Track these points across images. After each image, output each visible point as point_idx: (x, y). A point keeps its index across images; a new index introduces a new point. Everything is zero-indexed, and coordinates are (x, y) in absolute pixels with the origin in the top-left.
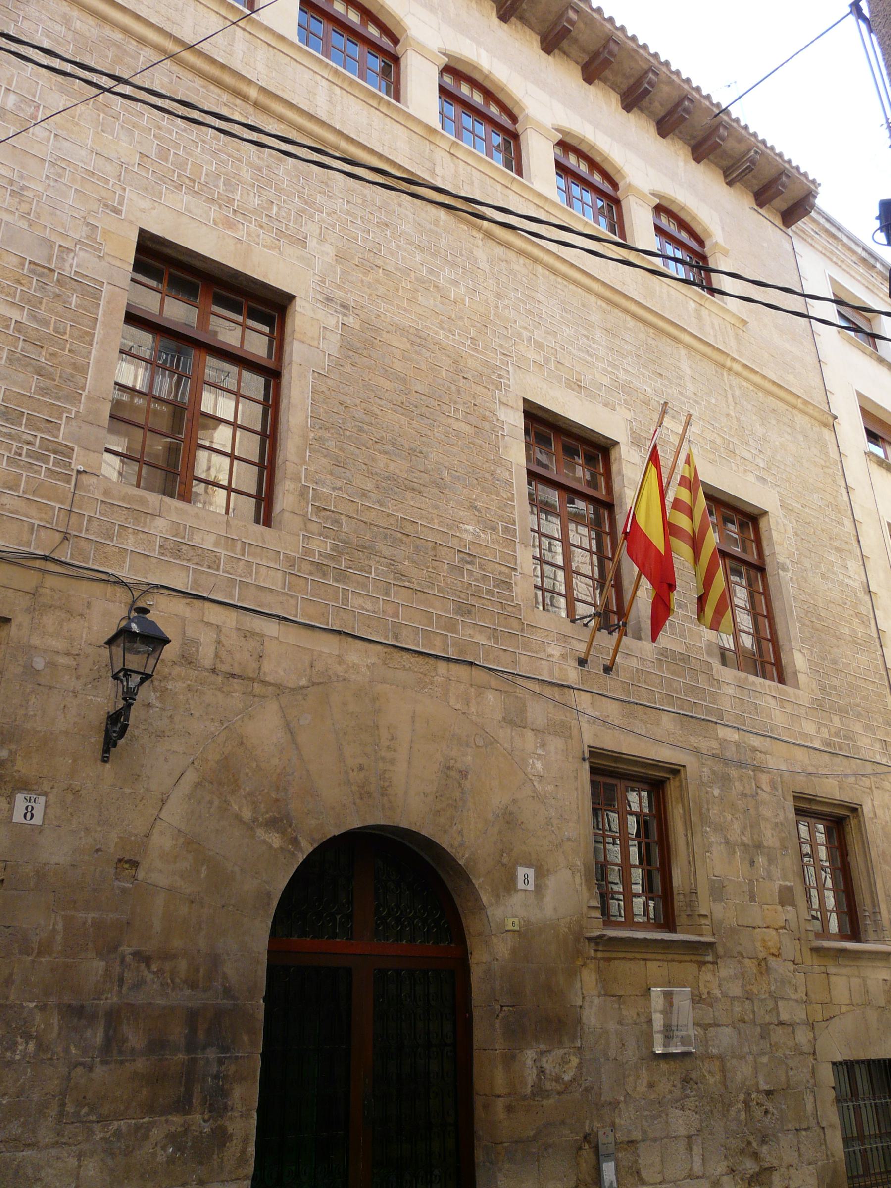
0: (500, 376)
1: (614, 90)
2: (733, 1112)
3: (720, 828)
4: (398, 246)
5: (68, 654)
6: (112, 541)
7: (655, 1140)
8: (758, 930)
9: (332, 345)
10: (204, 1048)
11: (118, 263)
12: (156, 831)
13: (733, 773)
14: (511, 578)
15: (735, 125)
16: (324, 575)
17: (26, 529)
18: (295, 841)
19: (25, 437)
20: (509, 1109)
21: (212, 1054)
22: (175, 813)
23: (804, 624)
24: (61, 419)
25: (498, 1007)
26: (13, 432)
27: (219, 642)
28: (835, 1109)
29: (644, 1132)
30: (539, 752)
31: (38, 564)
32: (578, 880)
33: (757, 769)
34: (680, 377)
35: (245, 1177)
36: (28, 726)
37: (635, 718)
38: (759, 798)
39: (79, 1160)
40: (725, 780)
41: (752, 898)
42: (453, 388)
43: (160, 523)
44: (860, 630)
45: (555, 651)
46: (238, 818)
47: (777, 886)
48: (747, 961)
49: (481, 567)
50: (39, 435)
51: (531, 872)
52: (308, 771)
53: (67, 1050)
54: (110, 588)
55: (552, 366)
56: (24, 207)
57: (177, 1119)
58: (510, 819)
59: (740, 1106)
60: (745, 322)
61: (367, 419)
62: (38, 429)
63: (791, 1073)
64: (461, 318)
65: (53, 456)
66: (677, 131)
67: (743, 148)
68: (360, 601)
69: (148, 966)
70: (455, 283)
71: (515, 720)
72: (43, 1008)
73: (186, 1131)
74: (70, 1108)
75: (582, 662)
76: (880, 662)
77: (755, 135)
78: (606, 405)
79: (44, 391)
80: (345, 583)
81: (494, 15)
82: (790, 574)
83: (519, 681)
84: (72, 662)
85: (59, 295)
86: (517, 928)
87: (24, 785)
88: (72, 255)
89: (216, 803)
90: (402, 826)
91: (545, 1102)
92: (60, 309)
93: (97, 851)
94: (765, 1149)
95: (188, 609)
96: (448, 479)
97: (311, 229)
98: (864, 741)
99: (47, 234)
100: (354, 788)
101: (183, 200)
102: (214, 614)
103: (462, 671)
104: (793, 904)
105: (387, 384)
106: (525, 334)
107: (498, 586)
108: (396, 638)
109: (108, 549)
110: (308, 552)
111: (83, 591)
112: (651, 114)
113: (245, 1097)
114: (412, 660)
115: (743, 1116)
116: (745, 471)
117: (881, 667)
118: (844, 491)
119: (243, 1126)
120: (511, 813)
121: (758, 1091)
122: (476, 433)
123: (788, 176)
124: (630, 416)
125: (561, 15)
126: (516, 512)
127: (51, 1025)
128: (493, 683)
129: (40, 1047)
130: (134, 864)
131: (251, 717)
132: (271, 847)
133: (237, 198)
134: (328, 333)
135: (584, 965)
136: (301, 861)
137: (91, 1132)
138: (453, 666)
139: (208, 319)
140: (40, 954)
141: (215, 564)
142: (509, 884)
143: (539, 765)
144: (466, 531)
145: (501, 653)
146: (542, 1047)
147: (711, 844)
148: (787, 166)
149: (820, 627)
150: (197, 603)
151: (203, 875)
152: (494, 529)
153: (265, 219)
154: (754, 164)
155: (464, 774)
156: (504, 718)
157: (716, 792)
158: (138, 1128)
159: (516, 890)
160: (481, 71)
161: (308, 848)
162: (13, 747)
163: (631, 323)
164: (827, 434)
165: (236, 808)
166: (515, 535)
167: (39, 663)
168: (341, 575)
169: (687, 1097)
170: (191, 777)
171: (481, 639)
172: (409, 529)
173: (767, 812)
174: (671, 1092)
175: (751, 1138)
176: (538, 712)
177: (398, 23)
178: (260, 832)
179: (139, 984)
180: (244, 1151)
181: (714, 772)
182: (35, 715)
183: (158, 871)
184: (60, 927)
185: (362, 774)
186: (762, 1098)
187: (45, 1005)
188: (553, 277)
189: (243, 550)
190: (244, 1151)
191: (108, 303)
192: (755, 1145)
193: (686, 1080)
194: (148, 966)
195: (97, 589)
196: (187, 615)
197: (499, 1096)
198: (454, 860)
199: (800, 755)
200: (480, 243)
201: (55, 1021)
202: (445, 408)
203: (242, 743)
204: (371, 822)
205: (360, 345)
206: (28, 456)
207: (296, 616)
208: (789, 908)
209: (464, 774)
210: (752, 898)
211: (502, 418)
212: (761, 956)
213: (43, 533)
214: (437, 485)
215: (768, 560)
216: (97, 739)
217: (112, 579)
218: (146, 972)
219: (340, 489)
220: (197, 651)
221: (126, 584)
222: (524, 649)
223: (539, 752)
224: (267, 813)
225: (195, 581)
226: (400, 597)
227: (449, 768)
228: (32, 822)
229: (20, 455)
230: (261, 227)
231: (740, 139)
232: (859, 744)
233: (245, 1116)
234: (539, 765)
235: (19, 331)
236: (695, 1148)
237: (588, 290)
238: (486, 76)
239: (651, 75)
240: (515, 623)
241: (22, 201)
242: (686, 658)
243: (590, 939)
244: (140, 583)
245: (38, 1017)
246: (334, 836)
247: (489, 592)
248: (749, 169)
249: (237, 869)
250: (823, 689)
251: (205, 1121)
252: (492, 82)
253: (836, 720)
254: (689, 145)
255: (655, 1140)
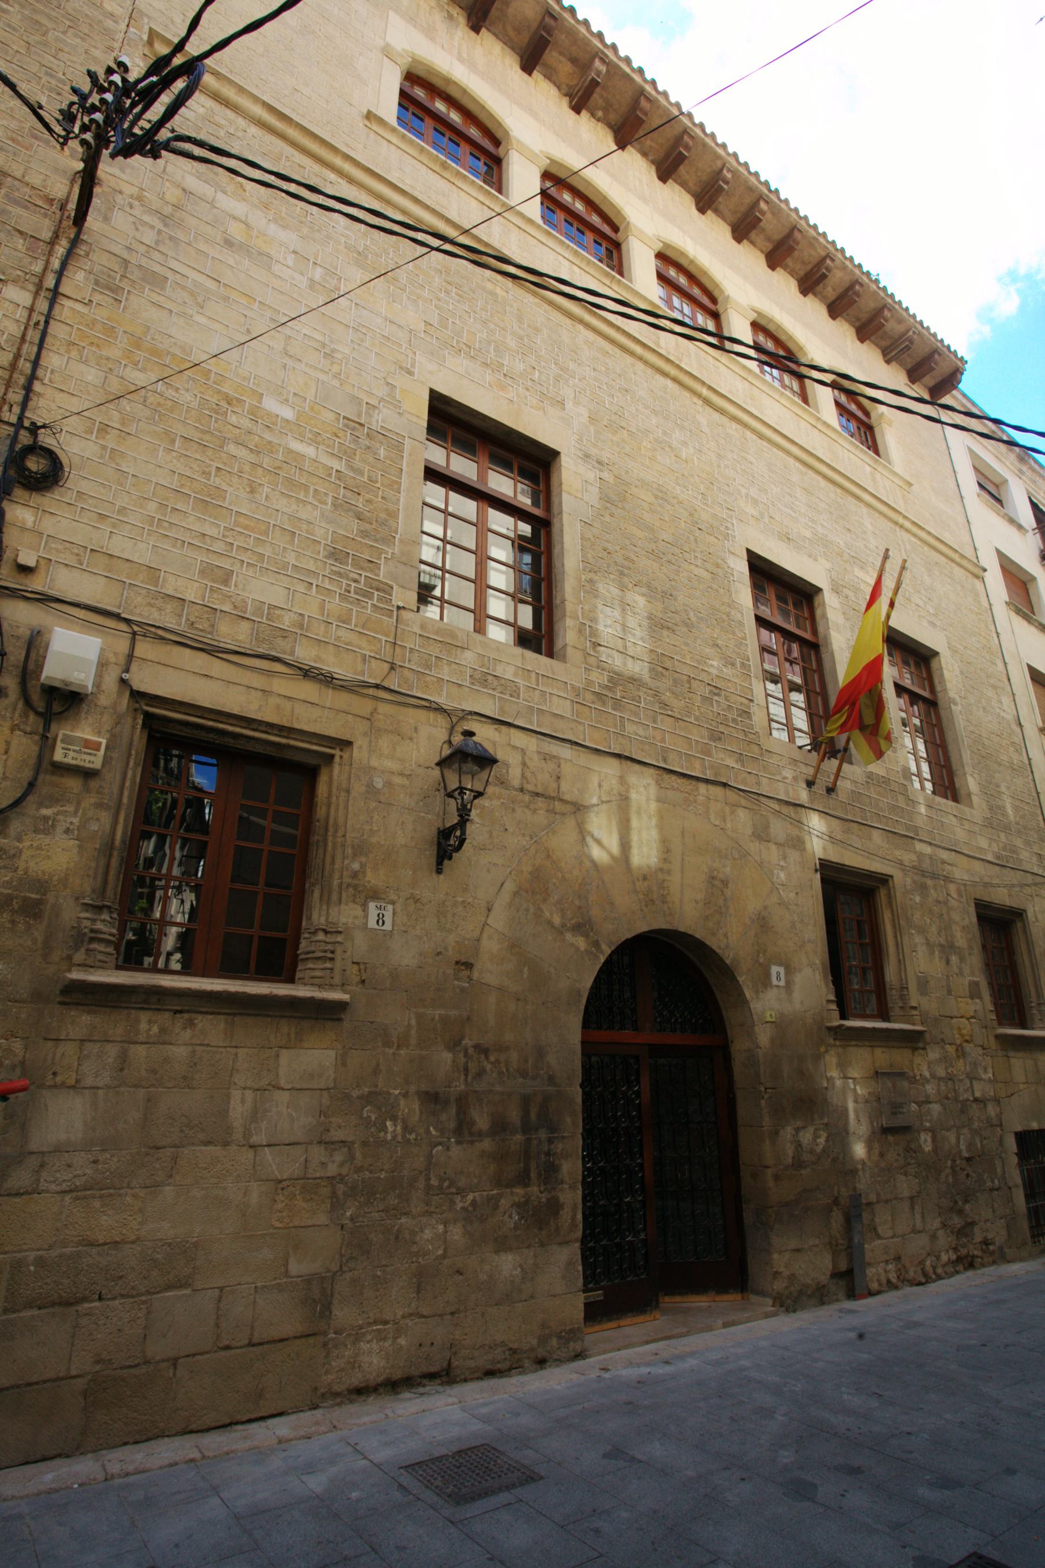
0: (727, 528)
1: (793, 276)
2: (943, 1175)
3: (922, 931)
4: (637, 410)
5: (401, 774)
6: (431, 670)
7: (887, 1201)
8: (954, 1020)
9: (592, 496)
10: (537, 1130)
11: (415, 419)
12: (485, 935)
13: (930, 882)
14: (749, 708)
15: (897, 307)
16: (604, 704)
17: (359, 659)
18: (596, 944)
19: (352, 575)
20: (777, 1178)
21: (543, 1134)
22: (498, 920)
23: (973, 752)
24: (380, 559)
25: (763, 1089)
26: (342, 571)
27: (524, 764)
28: (1018, 1172)
29: (878, 1195)
30: (782, 863)
31: (371, 691)
32: (818, 977)
33: (948, 879)
34: (864, 533)
35: (576, 1241)
36: (374, 840)
37: (852, 833)
38: (949, 904)
39: (445, 1226)
40: (923, 888)
41: (949, 992)
42: (692, 538)
43: (468, 654)
44: (1015, 757)
45: (788, 774)
46: (550, 923)
47: (966, 983)
48: (948, 1046)
49: (726, 699)
50: (364, 574)
51: (782, 970)
52: (603, 881)
53: (428, 1132)
54: (432, 715)
55: (766, 519)
56: (336, 368)
57: (519, 1191)
58: (763, 923)
59: (948, 1171)
60: (910, 484)
61: (626, 563)
62: (362, 569)
63: (985, 1142)
64: (692, 475)
65: (376, 593)
66: (844, 314)
67: (901, 328)
68: (634, 727)
69: (487, 1058)
70: (685, 443)
71: (761, 835)
72: (406, 1095)
73: (527, 1202)
74: (434, 1182)
75: (810, 784)
76: (1032, 785)
77: (914, 316)
78: (810, 556)
79: (364, 534)
80: (621, 711)
81: (693, 207)
82: (959, 708)
83: (762, 799)
84: (406, 782)
85: (369, 448)
86: (773, 1020)
87: (375, 895)
88: (377, 411)
89: (532, 910)
90: (697, 936)
91: (803, 1172)
92: (371, 459)
93: (439, 953)
94: (967, 1207)
95: (497, 734)
96: (694, 619)
97: (567, 392)
98: (1024, 855)
99: (356, 393)
100: (641, 896)
101: (460, 364)
102: (519, 739)
103: (718, 791)
104: (980, 998)
105: (639, 533)
106: (744, 491)
107: (740, 715)
108: (665, 761)
109: (428, 678)
110: (590, 682)
111: (412, 717)
112: (822, 298)
113: (572, 1168)
114: (679, 781)
115: (951, 1180)
116: (920, 616)
117: (1033, 790)
118: (995, 635)
119: (571, 1197)
120: (763, 918)
121: (961, 1158)
122: (713, 579)
123: (940, 354)
124: (828, 565)
125: (755, 205)
126: (749, 649)
127: (411, 1108)
128: (743, 802)
129: (406, 1129)
130: (469, 966)
131: (554, 833)
132: (578, 949)
133: (506, 363)
134: (589, 487)
135: (826, 1051)
136: (602, 961)
137: (452, 1203)
138: (710, 787)
139: (487, 473)
140: (399, 1047)
141: (515, 693)
142: (764, 981)
143: (782, 875)
144: (712, 666)
145: (747, 775)
146: (799, 1123)
147: (916, 945)
148: (939, 345)
149: (984, 754)
150: (504, 728)
151: (525, 976)
152: (733, 665)
153: (530, 383)
154: (912, 343)
155: (725, 883)
156: (753, 833)
157: (918, 899)
158: (489, 1199)
159: (771, 986)
160: (687, 256)
161: (608, 951)
162: (363, 859)
163: (823, 483)
164: (979, 585)
165: (548, 914)
166: (750, 671)
167: (379, 783)
168: (617, 704)
169: (909, 1164)
170: (510, 887)
171: (731, 762)
172: (668, 664)
173: (956, 916)
174: (897, 1160)
175: (957, 1198)
176: (779, 829)
177: (619, 212)
178: (568, 936)
179: (481, 1073)
180: (574, 1218)
181: (914, 882)
182: (379, 830)
183: (490, 970)
184: (413, 1022)
185: (646, 884)
186: (964, 1162)
187: (407, 1092)
188: (760, 441)
189: (537, 680)
190: (574, 1218)
191: (410, 455)
192: (960, 1203)
193: (908, 1150)
194: (487, 1058)
195: (422, 714)
196: (497, 739)
197: (767, 1167)
198: (721, 959)
199: (978, 866)
200: (701, 409)
201: (416, 1106)
202: (687, 555)
203: (549, 856)
204: (655, 926)
205: (614, 497)
206: (356, 593)
207: (584, 740)
208: (978, 1001)
209: (725, 883)
210: (949, 992)
211: (732, 566)
212: (958, 1042)
213: (374, 663)
214: (686, 625)
215: (940, 695)
216: (432, 853)
217: (434, 705)
218: (485, 1063)
219: (610, 626)
220: (507, 772)
221: (445, 711)
222: (764, 772)
223: (782, 863)
224: (572, 919)
225: (501, 709)
226: (666, 724)
227: (713, 878)
228: (383, 928)
229: (349, 592)
230: (528, 390)
231: (900, 321)
232: (1021, 857)
233: (573, 1187)
234: (782, 875)
235: (339, 479)
236: (916, 1207)
237: (788, 453)
238: (692, 262)
239: (828, 261)
240: (756, 748)
241: (333, 363)
242: (886, 781)
243: (830, 1029)
244: (456, 710)
245: (402, 1102)
246: (627, 940)
247: (734, 720)
248: (908, 348)
249: (552, 970)
250: (991, 809)
251: (541, 1192)
252: (697, 266)
253: (1002, 835)
254: (854, 326)
255: (887, 1201)
